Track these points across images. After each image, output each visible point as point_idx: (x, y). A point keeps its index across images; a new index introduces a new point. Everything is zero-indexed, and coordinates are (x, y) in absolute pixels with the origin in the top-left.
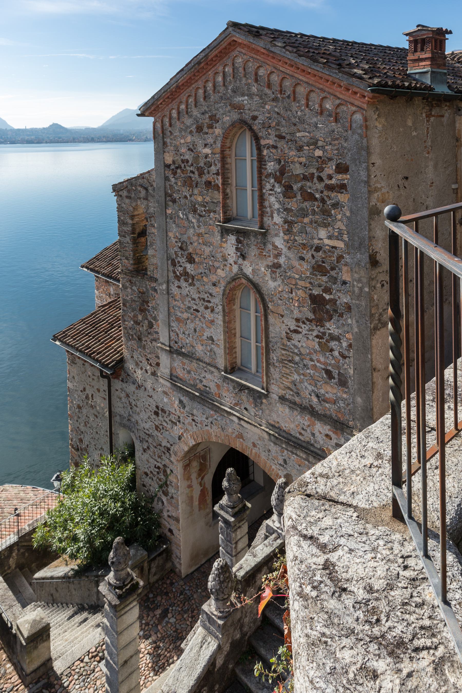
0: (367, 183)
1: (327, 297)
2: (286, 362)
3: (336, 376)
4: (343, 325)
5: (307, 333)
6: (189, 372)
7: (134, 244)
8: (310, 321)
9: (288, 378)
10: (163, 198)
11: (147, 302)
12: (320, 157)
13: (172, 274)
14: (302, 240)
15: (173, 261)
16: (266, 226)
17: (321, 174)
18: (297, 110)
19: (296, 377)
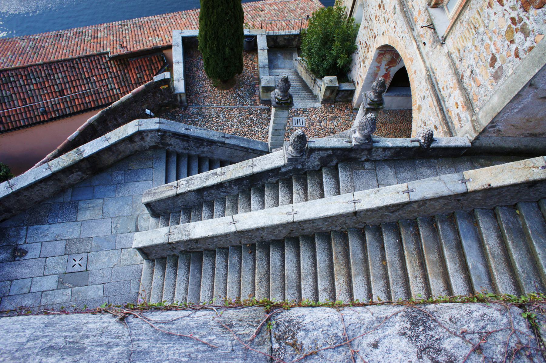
3: (496, 67)
5: (508, 9)
9: (463, 42)
19: (469, 45)
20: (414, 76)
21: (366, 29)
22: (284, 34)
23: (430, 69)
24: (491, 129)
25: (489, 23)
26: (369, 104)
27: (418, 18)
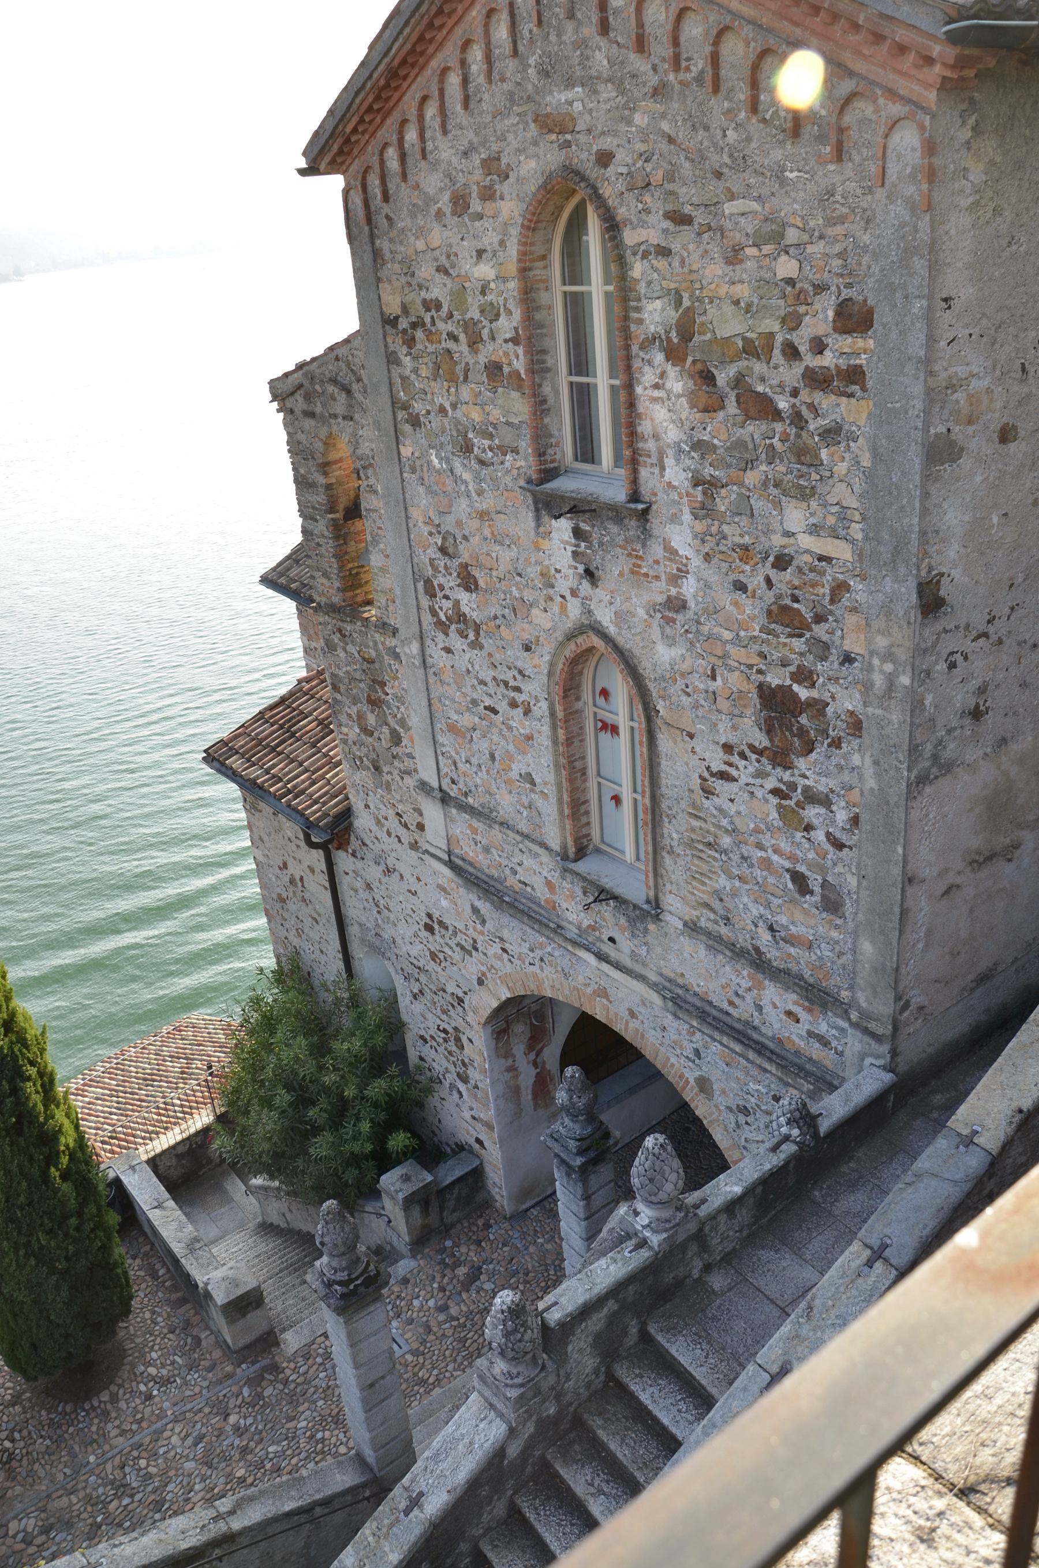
0: (927, 363)
1: (803, 693)
2: (701, 847)
3: (817, 889)
4: (840, 768)
5: (751, 781)
6: (487, 850)
7: (336, 538)
8: (760, 752)
9: (704, 884)
10: (389, 415)
11: (383, 684)
12: (790, 282)
13: (430, 617)
14: (742, 536)
15: (428, 582)
16: (645, 491)
17: (795, 338)
18: (725, 124)
19: (722, 882)
20: (634, 1024)
21: (421, 998)
22: (172, 1142)
23: (667, 984)
24: (906, 1014)
25: (732, 823)
26: (580, 1153)
27: (555, 898)
